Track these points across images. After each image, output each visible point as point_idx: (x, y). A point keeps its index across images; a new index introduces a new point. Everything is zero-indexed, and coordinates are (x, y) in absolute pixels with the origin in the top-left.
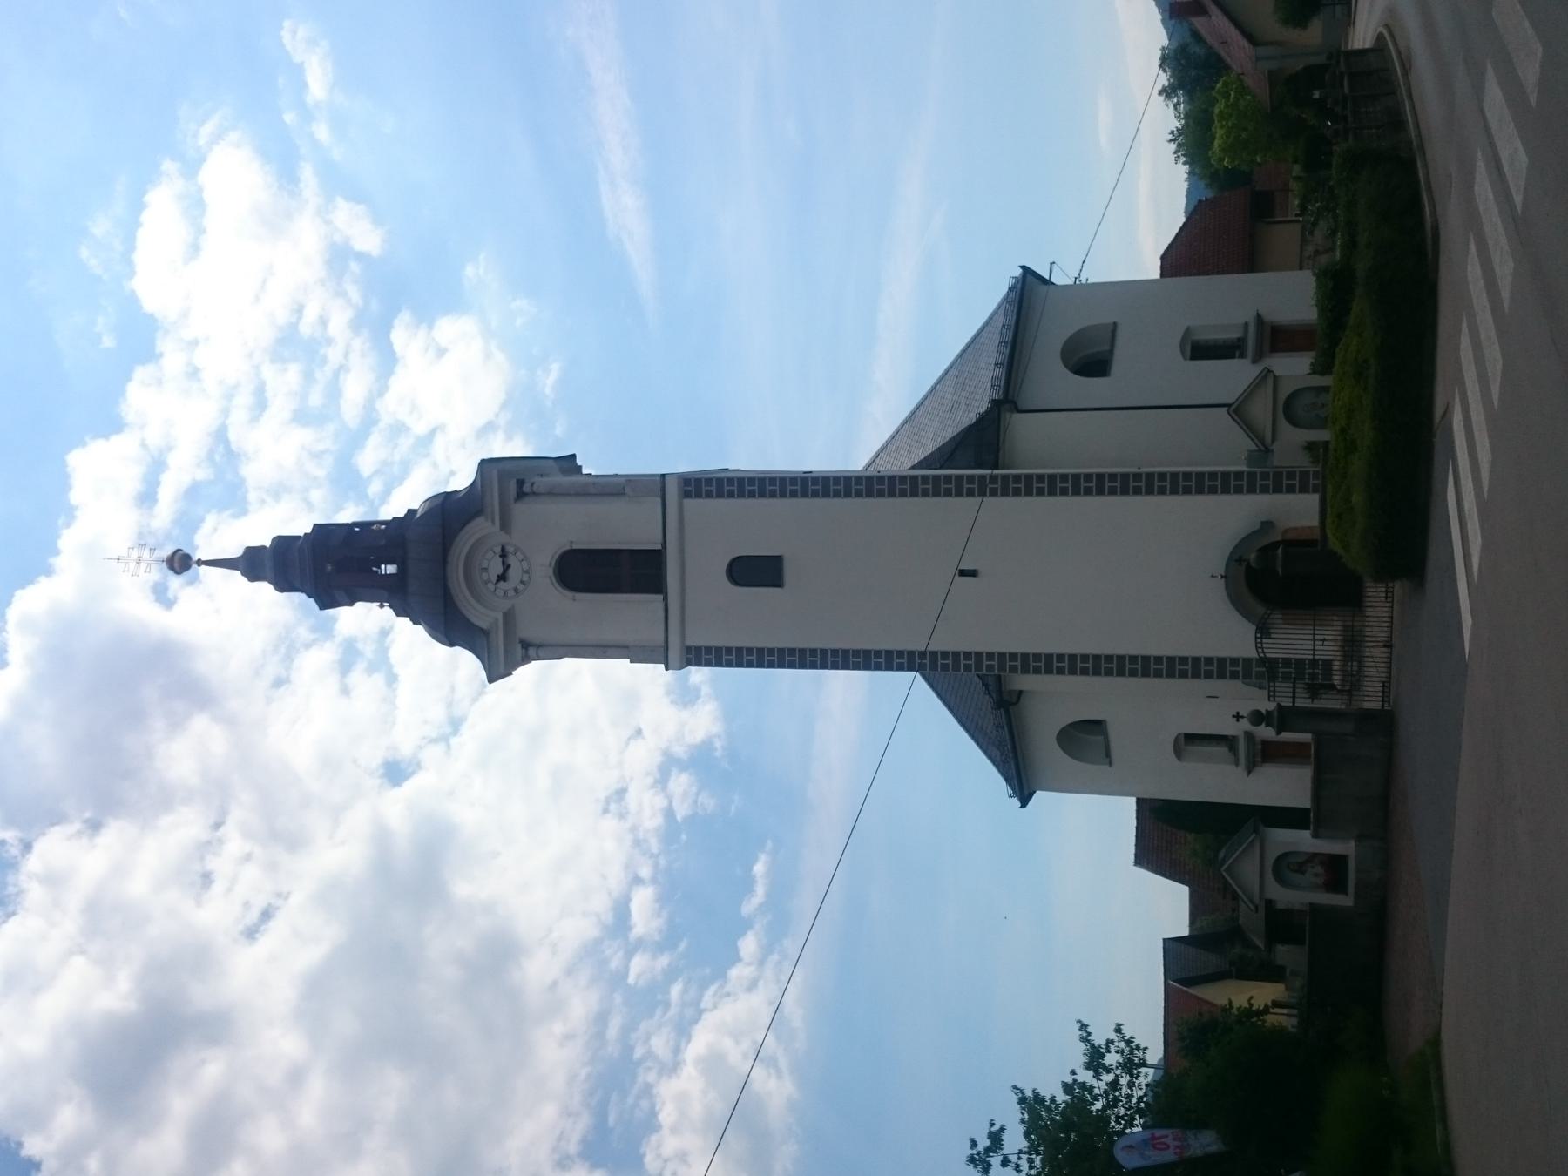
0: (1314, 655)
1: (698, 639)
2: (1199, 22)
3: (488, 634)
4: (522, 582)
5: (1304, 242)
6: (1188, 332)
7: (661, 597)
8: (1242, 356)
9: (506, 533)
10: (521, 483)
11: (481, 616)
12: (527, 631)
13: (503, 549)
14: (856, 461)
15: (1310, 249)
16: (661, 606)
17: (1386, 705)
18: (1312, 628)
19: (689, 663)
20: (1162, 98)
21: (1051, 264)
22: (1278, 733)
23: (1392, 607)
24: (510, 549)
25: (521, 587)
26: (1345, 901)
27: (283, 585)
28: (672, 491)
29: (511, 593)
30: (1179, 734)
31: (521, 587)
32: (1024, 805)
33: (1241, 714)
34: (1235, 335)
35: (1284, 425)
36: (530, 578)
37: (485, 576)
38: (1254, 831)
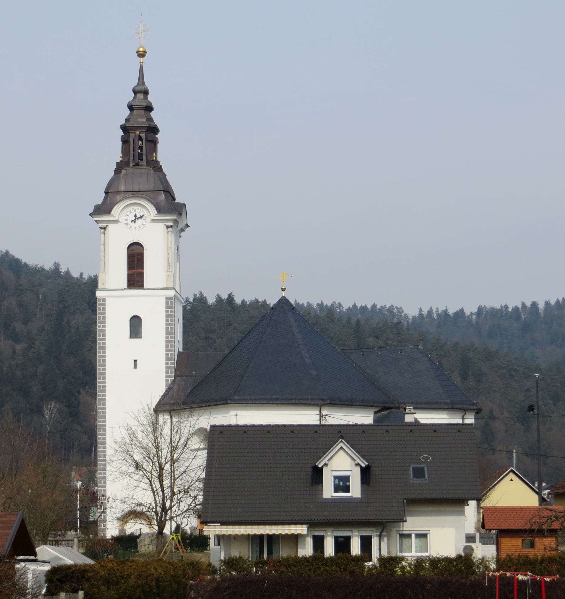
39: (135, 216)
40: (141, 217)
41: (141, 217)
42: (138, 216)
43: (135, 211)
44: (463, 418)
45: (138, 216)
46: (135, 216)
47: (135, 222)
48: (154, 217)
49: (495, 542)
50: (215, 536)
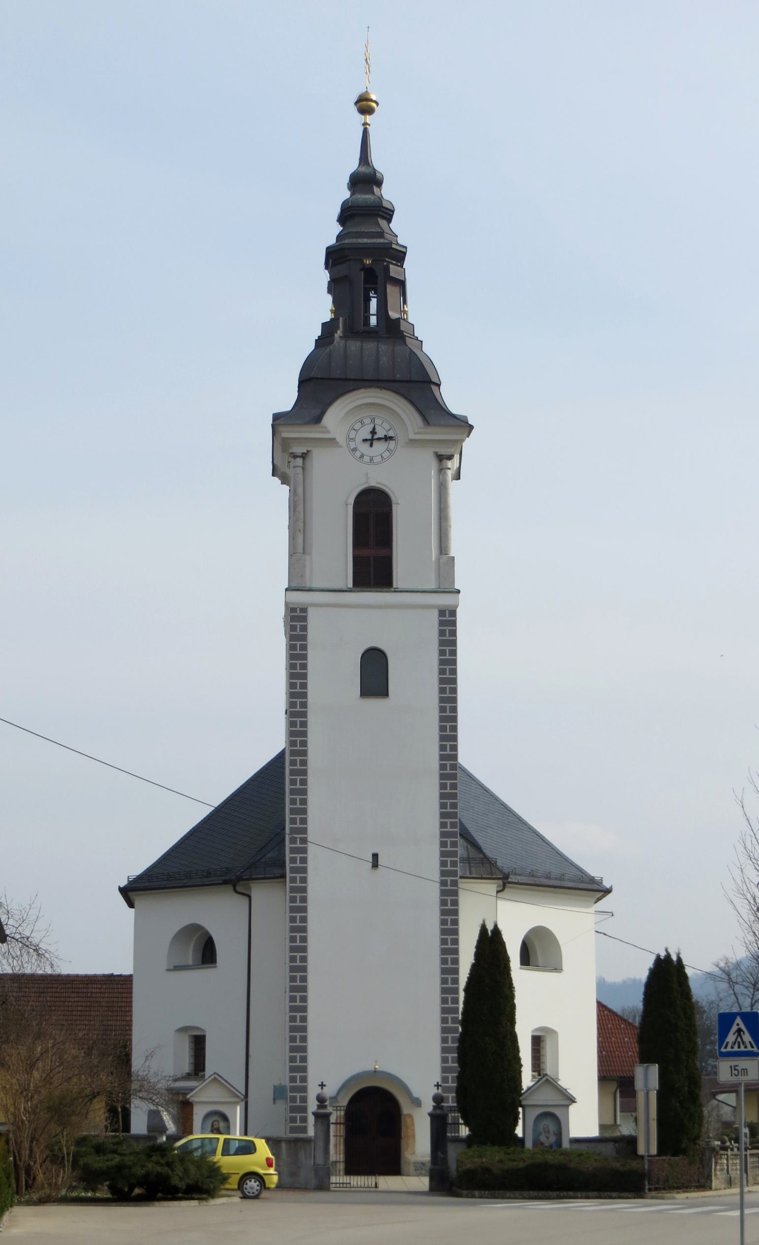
1: (314, 619)
13: (391, 438)
14: (466, 758)
16: (342, 586)
17: (334, 1185)
21: (611, 912)
22: (314, 1114)
24: (392, 443)
25: (358, 454)
28: (444, 600)
29: (352, 445)
30: (205, 1031)
33: (324, 1087)
39: (373, 432)
40: (387, 438)
41: (387, 438)
42: (380, 433)
43: (373, 420)
44: (336, 1124)
45: (380, 433)
46: (373, 432)
47: (371, 445)
48: (416, 433)
49: (608, 1135)
50: (521, 968)
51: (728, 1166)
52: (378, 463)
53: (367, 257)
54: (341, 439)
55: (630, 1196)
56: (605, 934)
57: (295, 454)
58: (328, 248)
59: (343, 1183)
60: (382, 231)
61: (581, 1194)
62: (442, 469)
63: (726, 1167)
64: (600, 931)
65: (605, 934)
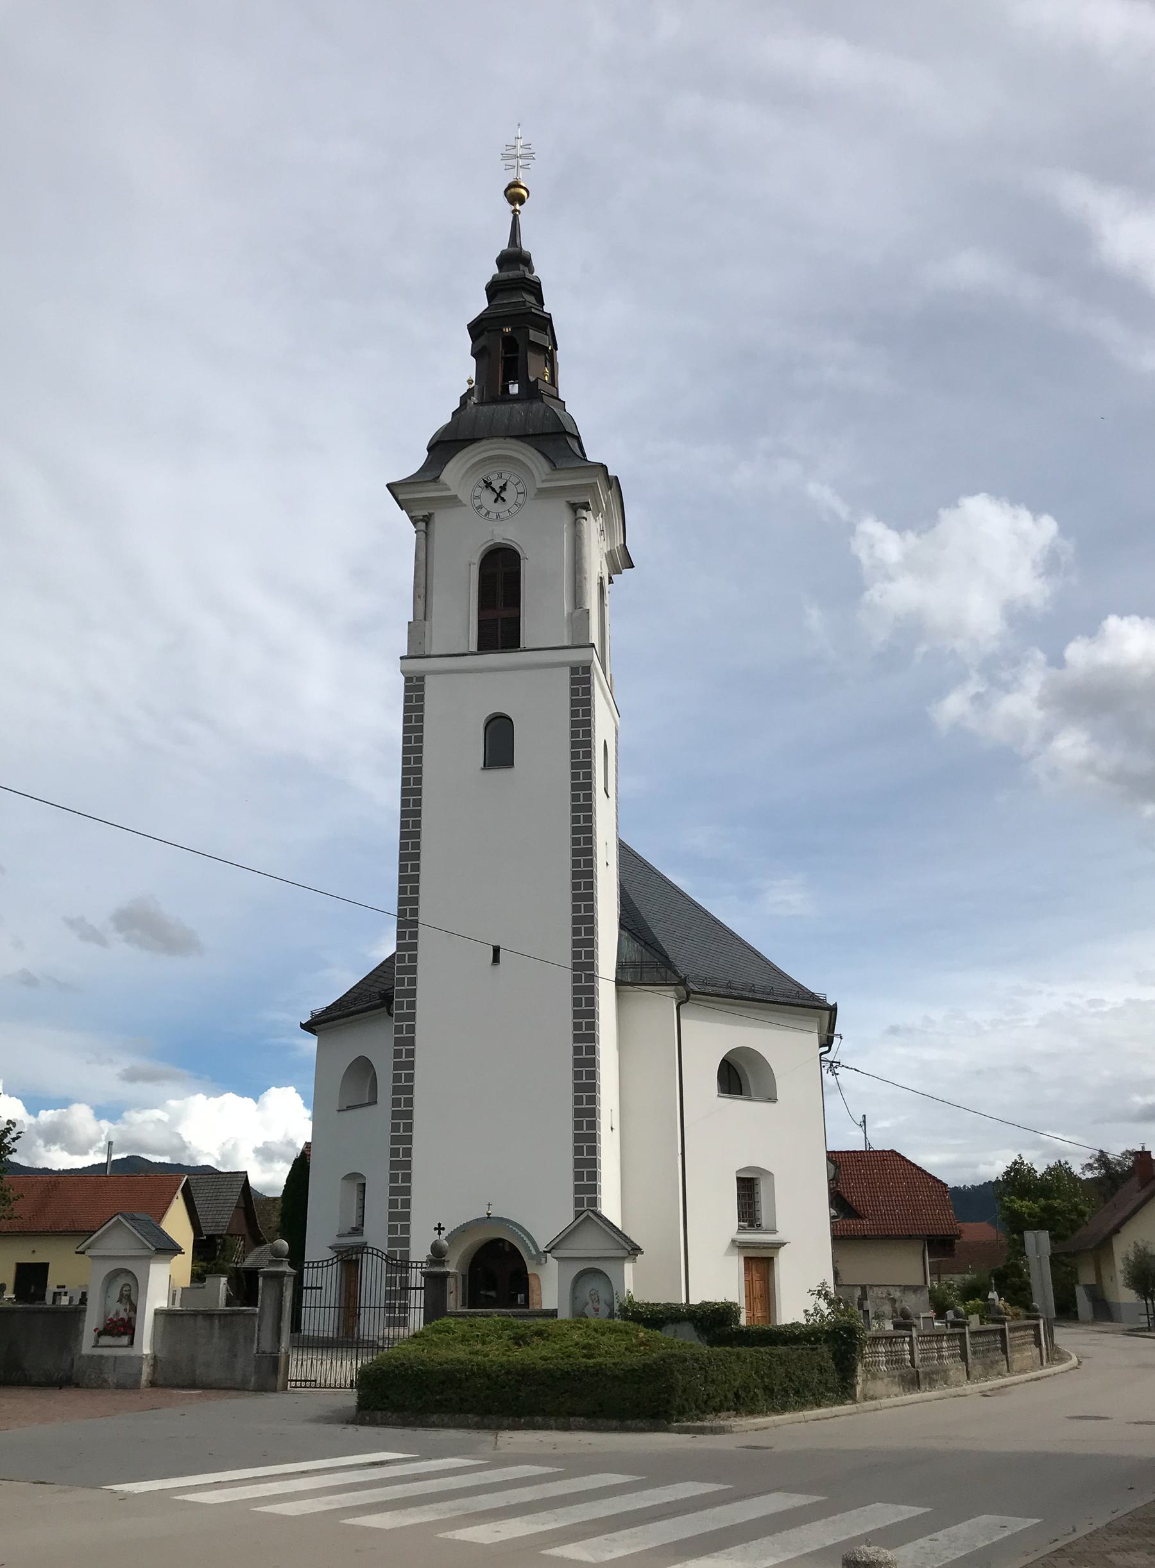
0: (420, 1308)
1: (432, 686)
2: (1135, 1181)
3: (435, 482)
4: (488, 513)
5: (906, 1288)
6: (768, 1174)
7: (474, 648)
8: (741, 1229)
9: (535, 495)
10: (586, 507)
11: (454, 472)
12: (442, 521)
15: (897, 1294)
17: (293, 1384)
18: (337, 1305)
19: (407, 680)
20: (1097, 1154)
23: (340, 1388)
25: (483, 511)
26: (87, 1345)
27: (494, 290)
29: (477, 503)
31: (483, 511)
32: (303, 1026)
34: (764, 1219)
35: (576, 1269)
36: (493, 520)
37: (520, 488)
38: (157, 1249)
48: (543, 481)
51: (912, 1353)
52: (506, 519)
53: (506, 326)
54: (464, 496)
55: (641, 1425)
56: (856, 1070)
57: (416, 518)
58: (468, 325)
59: (306, 1381)
60: (524, 300)
61: (556, 1421)
62: (576, 520)
63: (908, 1357)
64: (850, 1067)
65: (856, 1070)
